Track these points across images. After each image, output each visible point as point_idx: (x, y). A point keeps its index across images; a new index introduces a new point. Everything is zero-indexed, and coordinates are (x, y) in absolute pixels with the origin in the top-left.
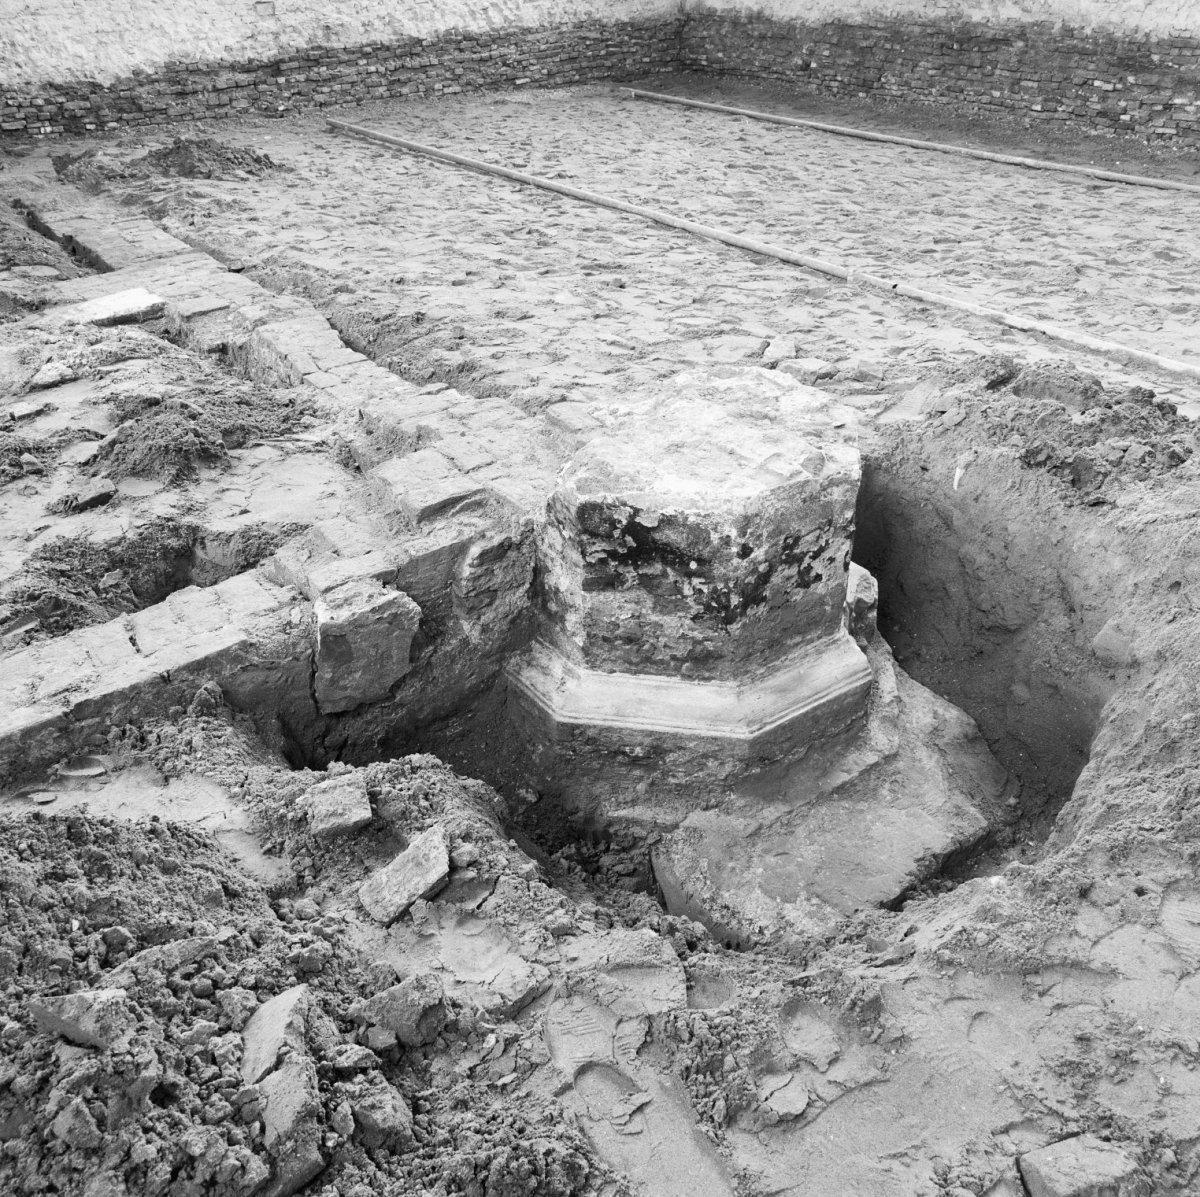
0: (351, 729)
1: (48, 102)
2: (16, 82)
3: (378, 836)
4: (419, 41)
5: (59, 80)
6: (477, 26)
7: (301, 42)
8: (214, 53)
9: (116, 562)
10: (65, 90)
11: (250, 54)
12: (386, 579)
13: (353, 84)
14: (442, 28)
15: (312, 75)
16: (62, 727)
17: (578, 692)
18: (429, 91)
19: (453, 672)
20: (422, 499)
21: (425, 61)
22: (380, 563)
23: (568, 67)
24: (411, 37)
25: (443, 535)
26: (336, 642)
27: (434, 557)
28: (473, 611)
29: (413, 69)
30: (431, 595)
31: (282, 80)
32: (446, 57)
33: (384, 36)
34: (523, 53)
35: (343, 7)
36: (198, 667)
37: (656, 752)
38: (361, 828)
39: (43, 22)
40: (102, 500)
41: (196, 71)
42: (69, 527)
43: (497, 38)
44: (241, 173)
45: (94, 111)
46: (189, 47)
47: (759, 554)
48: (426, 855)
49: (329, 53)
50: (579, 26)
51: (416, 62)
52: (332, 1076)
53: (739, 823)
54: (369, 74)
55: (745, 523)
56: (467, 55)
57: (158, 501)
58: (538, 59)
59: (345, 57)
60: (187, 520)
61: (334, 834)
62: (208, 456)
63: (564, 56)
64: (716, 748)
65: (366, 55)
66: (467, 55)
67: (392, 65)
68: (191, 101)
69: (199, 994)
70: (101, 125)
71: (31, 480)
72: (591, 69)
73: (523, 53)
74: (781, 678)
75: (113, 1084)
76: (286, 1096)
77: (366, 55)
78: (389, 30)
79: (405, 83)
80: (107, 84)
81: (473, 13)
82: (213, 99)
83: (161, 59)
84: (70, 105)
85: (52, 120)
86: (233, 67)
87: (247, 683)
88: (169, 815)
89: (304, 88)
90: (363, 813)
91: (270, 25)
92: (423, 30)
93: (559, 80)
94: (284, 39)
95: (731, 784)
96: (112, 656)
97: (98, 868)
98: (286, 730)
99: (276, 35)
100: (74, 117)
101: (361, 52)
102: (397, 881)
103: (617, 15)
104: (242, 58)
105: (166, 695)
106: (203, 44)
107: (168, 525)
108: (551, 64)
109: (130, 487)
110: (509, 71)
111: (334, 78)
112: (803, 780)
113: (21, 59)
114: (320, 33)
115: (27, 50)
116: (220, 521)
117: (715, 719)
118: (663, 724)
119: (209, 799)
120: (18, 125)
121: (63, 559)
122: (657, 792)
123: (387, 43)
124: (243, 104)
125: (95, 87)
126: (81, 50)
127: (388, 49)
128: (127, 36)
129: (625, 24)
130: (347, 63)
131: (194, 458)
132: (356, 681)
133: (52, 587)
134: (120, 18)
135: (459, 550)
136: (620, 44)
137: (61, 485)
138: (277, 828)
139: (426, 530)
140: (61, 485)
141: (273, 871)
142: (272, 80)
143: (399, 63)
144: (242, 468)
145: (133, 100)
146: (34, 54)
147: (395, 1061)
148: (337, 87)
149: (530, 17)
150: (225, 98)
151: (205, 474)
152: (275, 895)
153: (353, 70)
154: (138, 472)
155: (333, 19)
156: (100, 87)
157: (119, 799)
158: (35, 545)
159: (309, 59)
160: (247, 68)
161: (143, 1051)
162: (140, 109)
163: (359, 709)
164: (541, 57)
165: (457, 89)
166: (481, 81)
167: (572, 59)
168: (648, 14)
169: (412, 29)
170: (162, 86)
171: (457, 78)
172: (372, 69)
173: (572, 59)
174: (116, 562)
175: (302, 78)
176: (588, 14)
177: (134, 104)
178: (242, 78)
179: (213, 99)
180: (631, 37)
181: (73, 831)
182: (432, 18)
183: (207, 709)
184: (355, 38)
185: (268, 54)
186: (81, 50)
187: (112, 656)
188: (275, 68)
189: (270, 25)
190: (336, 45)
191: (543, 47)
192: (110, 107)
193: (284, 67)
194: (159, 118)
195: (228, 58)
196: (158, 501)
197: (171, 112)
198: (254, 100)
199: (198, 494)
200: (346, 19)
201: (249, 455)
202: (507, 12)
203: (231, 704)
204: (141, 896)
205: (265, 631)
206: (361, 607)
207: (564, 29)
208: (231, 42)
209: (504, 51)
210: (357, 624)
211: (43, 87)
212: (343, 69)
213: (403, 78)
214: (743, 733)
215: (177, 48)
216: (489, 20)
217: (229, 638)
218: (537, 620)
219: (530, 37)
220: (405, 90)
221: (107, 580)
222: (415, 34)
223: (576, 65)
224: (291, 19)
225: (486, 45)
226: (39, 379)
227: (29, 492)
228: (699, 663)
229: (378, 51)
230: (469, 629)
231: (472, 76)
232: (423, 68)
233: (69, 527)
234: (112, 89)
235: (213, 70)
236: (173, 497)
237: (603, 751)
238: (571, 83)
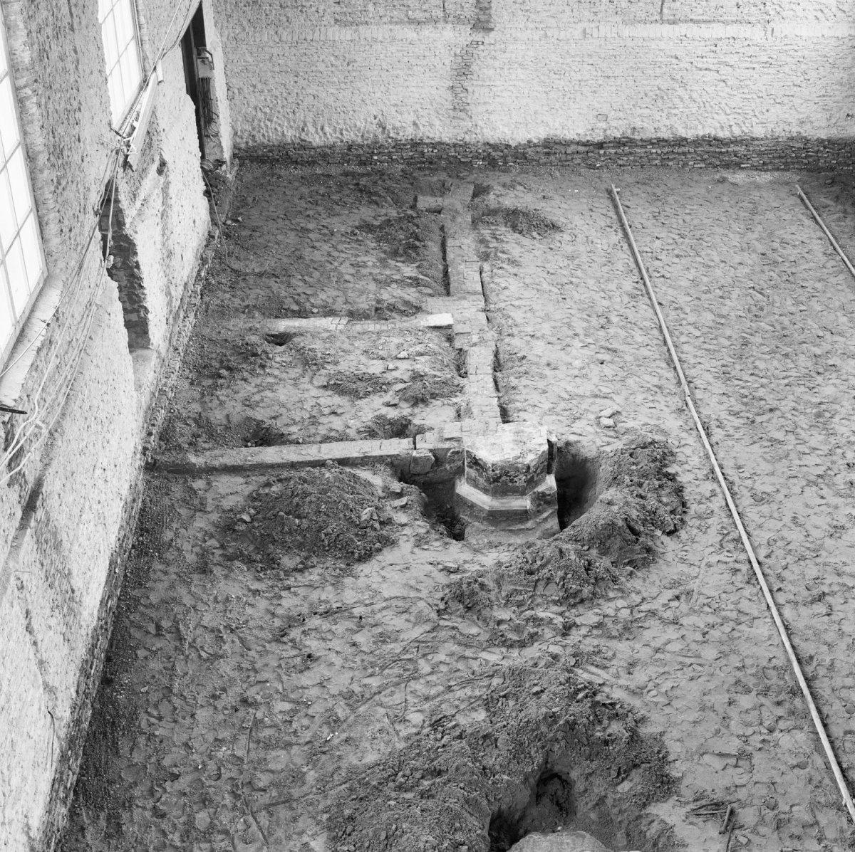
0: (417, 478)
1: (484, 151)
2: (473, 141)
3: (400, 495)
4: (686, 139)
7: (618, 135)
8: (570, 135)
10: (495, 147)
11: (589, 138)
12: (431, 451)
14: (701, 133)
16: (362, 459)
17: (464, 489)
18: (685, 164)
19: (440, 474)
21: (686, 149)
22: (431, 447)
24: (681, 137)
25: (447, 445)
26: (415, 460)
27: (443, 449)
30: (438, 458)
31: (602, 152)
32: (700, 149)
33: (665, 134)
36: (388, 456)
37: (472, 506)
38: (398, 493)
39: (492, 117)
41: (560, 143)
42: (384, 410)
43: (735, 141)
45: (504, 157)
46: (558, 132)
48: (404, 501)
50: (792, 139)
51: (680, 151)
53: (483, 527)
55: (493, 465)
56: (712, 149)
57: (405, 410)
60: (410, 418)
63: (776, 155)
64: (482, 510)
66: (712, 149)
67: (666, 150)
68: (552, 158)
69: (361, 503)
70: (506, 163)
71: (383, 393)
72: (793, 163)
76: (364, 517)
78: (669, 132)
79: (671, 160)
80: (513, 145)
82: (564, 157)
83: (543, 136)
84: (493, 154)
85: (483, 159)
86: (578, 143)
87: (396, 462)
88: (371, 480)
90: (399, 491)
91: (604, 125)
92: (690, 134)
93: (770, 167)
94: (608, 132)
95: (484, 519)
96: (376, 448)
97: (355, 482)
99: (605, 130)
100: (494, 159)
101: (650, 142)
102: (398, 503)
103: (818, 135)
104: (584, 140)
105: (381, 459)
106: (566, 132)
107: (404, 418)
110: (738, 160)
112: (503, 525)
113: (478, 131)
114: (629, 131)
115: (482, 128)
116: (416, 421)
117: (484, 503)
118: (475, 501)
119: (378, 480)
120: (468, 160)
124: (579, 161)
125: (508, 146)
127: (666, 141)
128: (529, 126)
129: (823, 141)
130: (641, 147)
132: (418, 469)
133: (374, 427)
134: (528, 118)
135: (449, 449)
136: (818, 151)
137: (388, 397)
138: (386, 488)
139: (66, 553)
140: (388, 397)
141: (382, 494)
143: (670, 149)
145: (524, 154)
146: (485, 130)
147: (381, 523)
148: (632, 158)
149: (759, 132)
150: (570, 157)
152: (380, 498)
153: (643, 150)
154: (406, 400)
156: (510, 146)
157: (364, 474)
158: (376, 414)
159: (618, 143)
160: (586, 144)
161: (351, 505)
162: (526, 158)
163: (419, 475)
164: (761, 154)
166: (718, 163)
168: (840, 136)
169: (682, 133)
172: (654, 151)
175: (613, 151)
176: (799, 133)
177: (524, 156)
178: (581, 149)
179: (564, 157)
180: (825, 148)
181: (354, 476)
182: (696, 129)
183: (387, 464)
184: (650, 134)
187: (376, 448)
188: (600, 145)
189: (604, 125)
190: (636, 137)
195: (577, 139)
196: (405, 410)
197: (541, 161)
198: (584, 160)
199: (416, 410)
200: (645, 125)
201: (438, 403)
202: (744, 129)
203: (392, 465)
204: (360, 489)
206: (422, 455)
207: (780, 140)
208: (581, 131)
209: (736, 148)
210: (420, 458)
211: (484, 144)
213: (671, 157)
214: (487, 508)
215: (552, 133)
216: (731, 132)
218: (460, 471)
219: (756, 142)
220: (671, 163)
221: (387, 427)
222: (684, 135)
224: (614, 123)
226: (399, 356)
228: (485, 491)
229: (660, 142)
230: (448, 467)
231: (714, 160)
232: (684, 153)
233: (384, 410)
234: (516, 148)
235: (568, 144)
236: (409, 410)
237: (463, 501)
238: (778, 169)
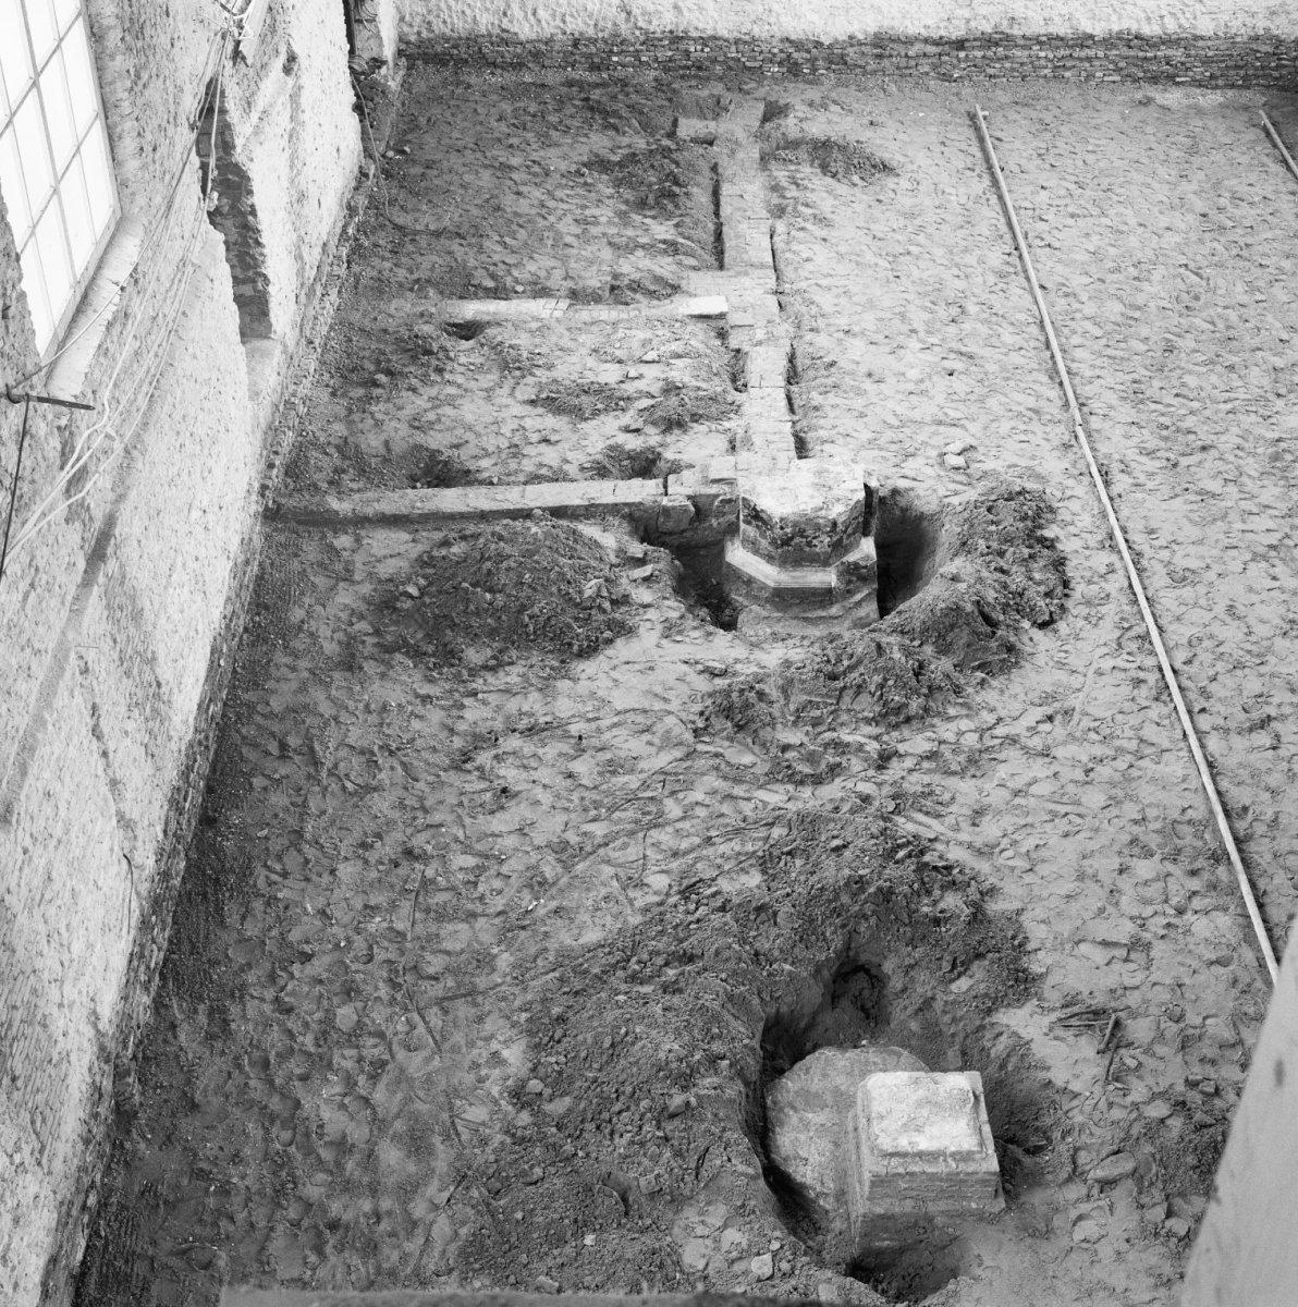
1: (781, 51)
2: (764, 35)
3: (642, 562)
4: (1092, 37)
5: (793, 37)
6: (1146, 31)
8: (913, 28)
9: (630, 457)
10: (798, 45)
12: (689, 497)
13: (1022, 64)
14: (1116, 28)
15: (990, 53)
16: (587, 508)
18: (1090, 76)
20: (714, 475)
21: (1091, 53)
22: (690, 492)
23: (1232, 72)
25: (714, 489)
26: (666, 511)
28: (717, 517)
29: (1080, 59)
30: (701, 509)
31: (962, 54)
33: (1061, 29)
34: (1189, 56)
35: (1030, 4)
36: (626, 504)
40: (637, 431)
42: (622, 438)
44: (856, 178)
45: (813, 61)
46: (896, 24)
47: (788, 530)
48: (647, 570)
49: (1008, 38)
52: (599, 595)
54: (1038, 58)
55: (782, 519)
56: (1132, 53)
57: (653, 437)
58: (1203, 63)
59: (1022, 42)
61: (633, 558)
62: (680, 424)
64: (764, 587)
65: (1040, 43)
67: (1062, 52)
68: (886, 62)
70: (814, 70)
73: (1189, 56)
74: (797, 574)
75: (562, 575)
76: (588, 593)
77: (1040, 43)
78: (1067, 24)
81: (1149, 19)
82: (903, 62)
83: (872, 29)
84: (795, 55)
85: (780, 64)
86: (926, 41)
87: (637, 514)
89: (979, 62)
92: (1098, 29)
93: (1220, 82)
94: (973, 24)
95: (767, 600)
97: (575, 541)
98: (646, 530)
99: (968, 21)
100: (796, 64)
105: (614, 509)
106: (908, 23)
107: (651, 449)
108: (1214, 68)
109: (650, 430)
110: (1171, 70)
111: (1007, 57)
113: (772, 20)
114: (1005, 22)
119: (610, 538)
120: (757, 64)
121: (615, 452)
122: (747, 595)
123: (1061, 34)
125: (818, 44)
126: (815, 18)
127: (1062, 39)
128: (852, 12)
130: (1023, 47)
131: (673, 424)
132: (670, 525)
133: (606, 462)
135: (717, 496)
137: (628, 419)
138: (621, 552)
140: (628, 419)
141: (614, 560)
142: (955, 53)
144: (691, 433)
145: (842, 56)
146: (783, 19)
148: (1008, 65)
149: (1205, 27)
150: (913, 63)
151: (676, 431)
153: (1026, 53)
154: (654, 423)
155: (1019, 13)
156: (822, 44)
157: (589, 530)
159: (988, 41)
160: (938, 42)
164: (1207, 61)
165: (1117, 78)
167: (1237, 67)
169: (1087, 26)
170: (866, 49)
171: (1118, 70)
173: (1237, 67)
174: (630, 457)
177: (843, 60)
179: (903, 62)
181: (574, 532)
183: (623, 517)
184: (1036, 27)
185: (957, 33)
186: (815, 18)
188: (960, 44)
189: (966, 13)
191: (1210, 54)
192: (824, 59)
193: (967, 44)
194: (858, 70)
195: (925, 33)
196: (653, 437)
198: (935, 67)
199: (669, 439)
200: (1030, 14)
202: (1183, 21)
204: (582, 550)
205: (648, 501)
206: (676, 504)
207: (1239, 39)
208: (930, 22)
209: (1170, 52)
210: (674, 508)
211: (782, 41)
212: (1017, 52)
213: (1068, 64)
214: (772, 585)
215: (886, 23)
216: (1163, 26)
217: (637, 500)
218: (732, 530)
220: (1067, 74)
222: (1089, 31)
223: (1242, 73)
225: (1154, 46)
226: (645, 358)
227: (617, 417)
228: (770, 559)
229: (1054, 41)
230: (714, 522)
231: (1134, 70)
232: (1089, 59)
233: (622, 438)
234: (830, 47)
235: (909, 41)
236: (659, 438)
237: (735, 574)
238: (1232, 86)
